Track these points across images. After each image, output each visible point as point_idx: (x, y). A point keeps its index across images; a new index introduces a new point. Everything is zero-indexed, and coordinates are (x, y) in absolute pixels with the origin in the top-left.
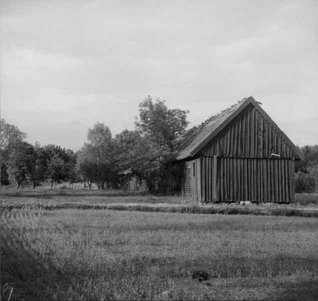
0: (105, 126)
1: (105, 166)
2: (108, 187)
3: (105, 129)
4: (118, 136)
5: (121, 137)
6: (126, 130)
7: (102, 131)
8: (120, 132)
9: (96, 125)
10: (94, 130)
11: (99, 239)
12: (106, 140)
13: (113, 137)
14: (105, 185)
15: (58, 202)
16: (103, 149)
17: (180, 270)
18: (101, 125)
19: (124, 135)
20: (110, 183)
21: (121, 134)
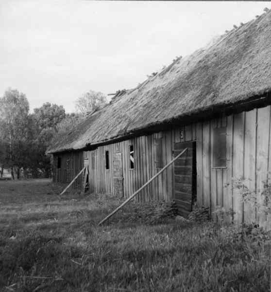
0: (20, 94)
1: (21, 145)
2: (26, 173)
3: (19, 98)
4: (37, 110)
5: (42, 111)
6: (48, 103)
7: (15, 100)
8: (39, 106)
9: (6, 92)
10: (4, 98)
11: (268, 74)
12: (22, 110)
13: (31, 112)
14: (22, 174)
15: (239, 259)
16: (79, 268)
17: (37, 230)
18: (14, 91)
19: (46, 109)
20: (28, 170)
21: (42, 108)
